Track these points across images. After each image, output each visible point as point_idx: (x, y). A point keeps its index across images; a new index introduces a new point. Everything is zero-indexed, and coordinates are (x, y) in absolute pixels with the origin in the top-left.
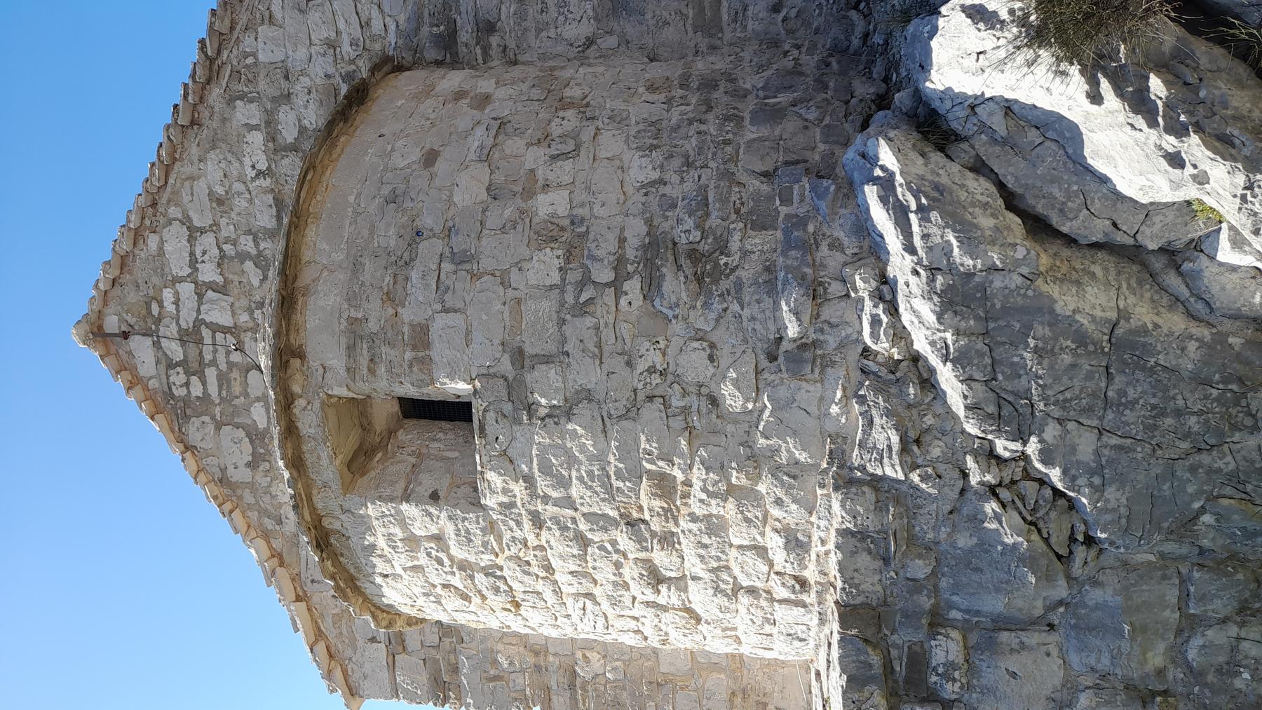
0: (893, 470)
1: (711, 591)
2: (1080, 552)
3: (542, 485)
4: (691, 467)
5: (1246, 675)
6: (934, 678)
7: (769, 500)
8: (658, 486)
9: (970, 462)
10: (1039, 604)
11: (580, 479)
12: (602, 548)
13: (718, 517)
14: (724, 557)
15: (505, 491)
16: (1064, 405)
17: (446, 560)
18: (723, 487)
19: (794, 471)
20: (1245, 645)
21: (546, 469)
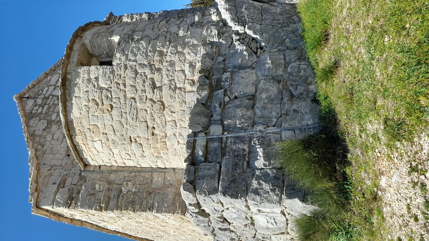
0: (216, 40)
1: (169, 88)
2: (259, 51)
3: (131, 57)
4: (168, 48)
5: (303, 72)
6: (223, 83)
7: (186, 54)
8: (160, 54)
9: (233, 35)
10: (250, 63)
11: (140, 54)
12: (141, 75)
13: (173, 61)
14: (173, 75)
15: (120, 59)
16: (252, 19)
17: (96, 86)
18: (175, 51)
19: (193, 46)
20: (301, 66)
21: (132, 52)
